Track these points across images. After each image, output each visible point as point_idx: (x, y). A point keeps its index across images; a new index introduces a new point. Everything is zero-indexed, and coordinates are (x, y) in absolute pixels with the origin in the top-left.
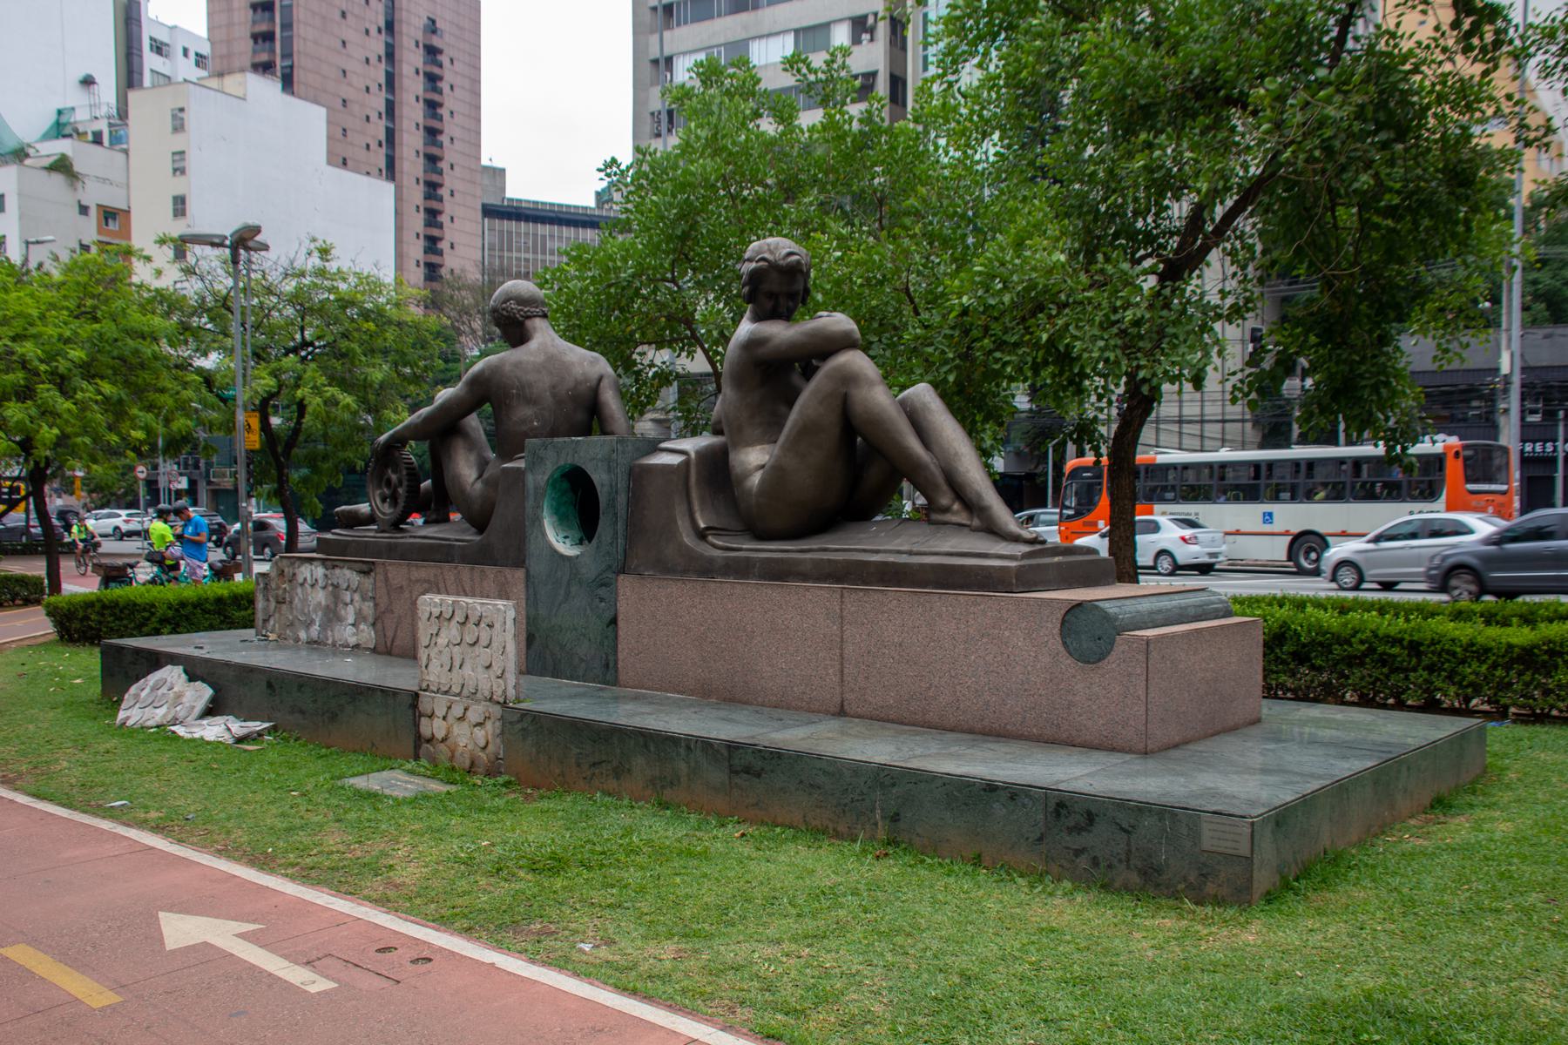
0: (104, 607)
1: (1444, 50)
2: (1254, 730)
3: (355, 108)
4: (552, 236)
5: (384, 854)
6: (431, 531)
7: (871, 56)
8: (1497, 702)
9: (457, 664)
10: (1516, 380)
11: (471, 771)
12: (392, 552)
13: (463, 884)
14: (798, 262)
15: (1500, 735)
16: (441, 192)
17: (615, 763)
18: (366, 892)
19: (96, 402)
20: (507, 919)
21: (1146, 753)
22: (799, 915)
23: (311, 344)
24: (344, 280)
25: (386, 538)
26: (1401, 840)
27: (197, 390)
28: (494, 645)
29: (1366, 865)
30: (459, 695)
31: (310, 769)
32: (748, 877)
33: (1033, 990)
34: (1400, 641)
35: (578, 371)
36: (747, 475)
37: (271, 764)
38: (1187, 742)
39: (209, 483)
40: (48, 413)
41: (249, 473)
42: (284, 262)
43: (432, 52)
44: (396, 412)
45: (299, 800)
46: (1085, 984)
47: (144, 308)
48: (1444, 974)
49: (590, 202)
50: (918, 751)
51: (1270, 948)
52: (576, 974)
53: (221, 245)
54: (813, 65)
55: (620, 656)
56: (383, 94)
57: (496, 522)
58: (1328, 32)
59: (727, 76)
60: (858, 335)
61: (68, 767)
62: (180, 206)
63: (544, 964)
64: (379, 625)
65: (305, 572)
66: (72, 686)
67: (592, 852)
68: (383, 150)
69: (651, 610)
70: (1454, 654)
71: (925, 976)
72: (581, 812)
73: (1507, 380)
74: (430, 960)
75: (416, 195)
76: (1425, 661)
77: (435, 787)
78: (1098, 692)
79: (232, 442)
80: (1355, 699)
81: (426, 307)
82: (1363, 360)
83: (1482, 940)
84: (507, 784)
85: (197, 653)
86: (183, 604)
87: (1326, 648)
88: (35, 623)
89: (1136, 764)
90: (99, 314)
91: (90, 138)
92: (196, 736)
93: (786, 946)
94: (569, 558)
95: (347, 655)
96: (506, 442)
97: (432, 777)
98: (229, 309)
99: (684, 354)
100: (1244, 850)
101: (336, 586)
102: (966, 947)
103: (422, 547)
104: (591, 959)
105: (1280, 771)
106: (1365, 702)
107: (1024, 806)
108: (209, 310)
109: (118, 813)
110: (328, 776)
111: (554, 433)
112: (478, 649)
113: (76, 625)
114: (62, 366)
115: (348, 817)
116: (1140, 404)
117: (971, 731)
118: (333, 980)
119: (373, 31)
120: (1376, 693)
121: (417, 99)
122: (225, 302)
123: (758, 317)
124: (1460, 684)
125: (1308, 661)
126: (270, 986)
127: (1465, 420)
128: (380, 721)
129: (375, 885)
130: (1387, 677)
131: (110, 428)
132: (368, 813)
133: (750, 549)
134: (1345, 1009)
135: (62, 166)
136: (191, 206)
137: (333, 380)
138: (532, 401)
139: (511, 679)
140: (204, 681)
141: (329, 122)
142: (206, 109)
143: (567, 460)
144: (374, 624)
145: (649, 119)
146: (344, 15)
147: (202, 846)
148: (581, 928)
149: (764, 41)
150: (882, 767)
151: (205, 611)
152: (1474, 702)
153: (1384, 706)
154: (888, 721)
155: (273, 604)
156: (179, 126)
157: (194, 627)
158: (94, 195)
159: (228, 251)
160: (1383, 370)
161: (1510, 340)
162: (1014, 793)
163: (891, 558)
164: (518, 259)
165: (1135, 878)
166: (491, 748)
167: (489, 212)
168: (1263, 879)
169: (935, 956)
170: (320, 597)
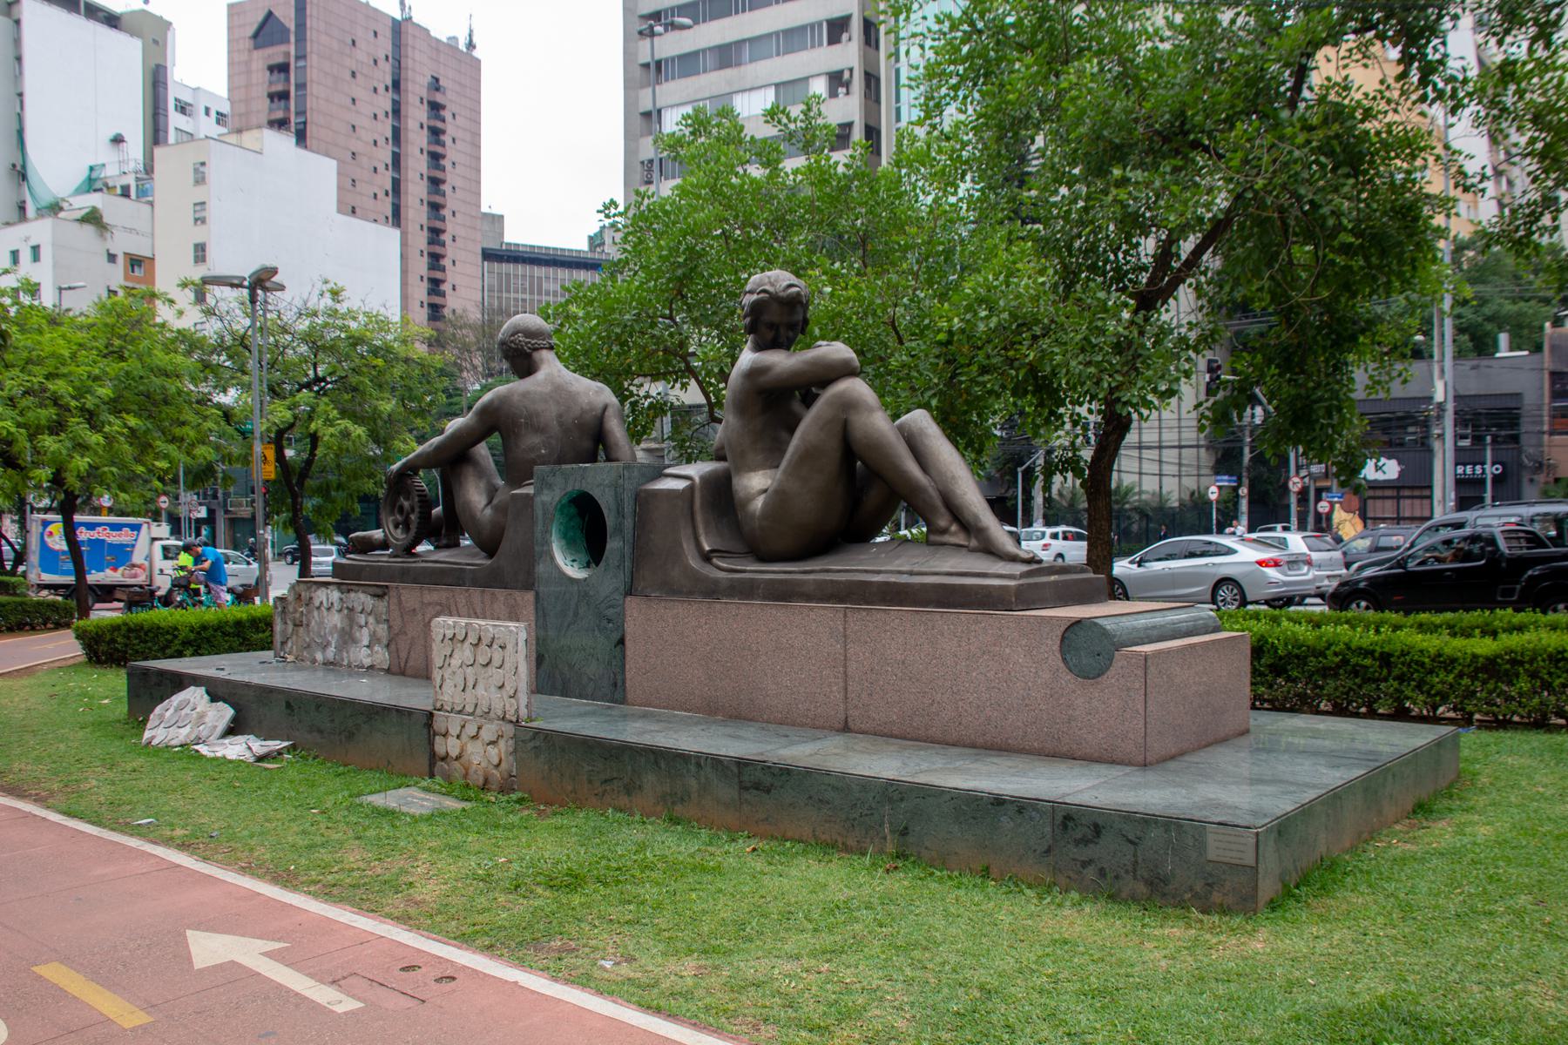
0: (130, 630)
1: (1389, 102)
2: (1243, 741)
3: (364, 160)
4: (548, 278)
5: (403, 871)
6: (443, 555)
7: (846, 109)
8: (1462, 709)
9: (470, 684)
10: (1450, 407)
11: (485, 787)
12: (406, 576)
13: (482, 901)
14: (798, 294)
15: (1471, 739)
16: (443, 237)
17: (626, 780)
18: (387, 909)
19: (122, 434)
20: (528, 936)
21: (1145, 765)
22: (815, 930)
23: (324, 379)
24: (354, 319)
25: (400, 563)
26: (1390, 845)
27: (217, 423)
28: (507, 665)
29: (1361, 871)
30: (472, 714)
31: (329, 786)
32: (762, 892)
33: (1053, 1004)
34: (1372, 653)
35: (584, 401)
36: (750, 499)
37: (291, 782)
38: (1182, 754)
39: (227, 512)
40: (81, 447)
41: (266, 503)
42: (298, 303)
43: (435, 107)
44: (404, 442)
45: (319, 818)
46: (1104, 996)
47: (169, 348)
48: (1450, 978)
49: (583, 246)
50: (924, 766)
51: (1279, 955)
52: (600, 993)
54: (793, 115)
55: (628, 676)
56: (390, 147)
57: (505, 546)
58: (1284, 83)
59: (715, 129)
60: (857, 364)
61: (97, 785)
62: (200, 253)
63: (567, 982)
64: (393, 647)
65: (321, 596)
66: (100, 706)
67: (608, 868)
68: (390, 199)
69: (659, 631)
70: (1423, 665)
71: (946, 990)
72: (595, 828)
73: (1441, 407)
74: (454, 979)
75: (420, 240)
76: (1396, 672)
77: (451, 804)
78: (1098, 706)
79: (248, 474)
80: (1329, 708)
81: (430, 345)
82: (1318, 385)
83: (1481, 943)
84: (520, 801)
85: (221, 675)
86: (204, 627)
87: (1301, 660)
88: (63, 646)
89: (1137, 776)
90: (126, 354)
91: (119, 191)
92: (219, 754)
93: (805, 962)
94: (576, 581)
95: (363, 675)
96: (515, 471)
97: (447, 794)
98: (246, 347)
99: (678, 385)
100: (1249, 859)
101: (351, 610)
102: (983, 960)
103: (433, 571)
104: (613, 977)
105: (1275, 781)
106: (1340, 711)
107: (1031, 818)
108: (228, 348)
109: (145, 830)
110: (346, 793)
111: (561, 460)
112: (491, 670)
113: (103, 647)
114: (90, 402)
115: (368, 834)
116: (1114, 429)
117: (973, 746)
118: (359, 999)
119: (381, 90)
120: (1349, 703)
122: (242, 341)
123: (759, 347)
124: (1428, 693)
125: (1289, 677)
126: (297, 1006)
127: (1402, 445)
128: (394, 740)
129: (396, 902)
130: (1360, 687)
131: (138, 460)
132: (386, 829)
133: (754, 570)
134: (1363, 1017)
136: (211, 253)
137: (344, 413)
138: (540, 430)
139: (523, 698)
140: (225, 701)
141: (339, 174)
142: (226, 163)
143: (574, 486)
144: (388, 646)
145: (639, 167)
146: (353, 74)
147: (227, 864)
148: (601, 945)
149: (746, 95)
150: (890, 783)
151: (224, 634)
152: (1441, 709)
153: (1357, 715)
154: (892, 736)
155: (290, 627)
156: (200, 179)
157: (216, 650)
158: (122, 244)
159: (245, 292)
160: (1335, 395)
161: (1442, 371)
162: (1022, 806)
163: (893, 579)
164: (516, 300)
165: (1142, 888)
166: (504, 766)
167: (489, 255)
168: (1268, 888)
169: (954, 971)
170: (335, 619)
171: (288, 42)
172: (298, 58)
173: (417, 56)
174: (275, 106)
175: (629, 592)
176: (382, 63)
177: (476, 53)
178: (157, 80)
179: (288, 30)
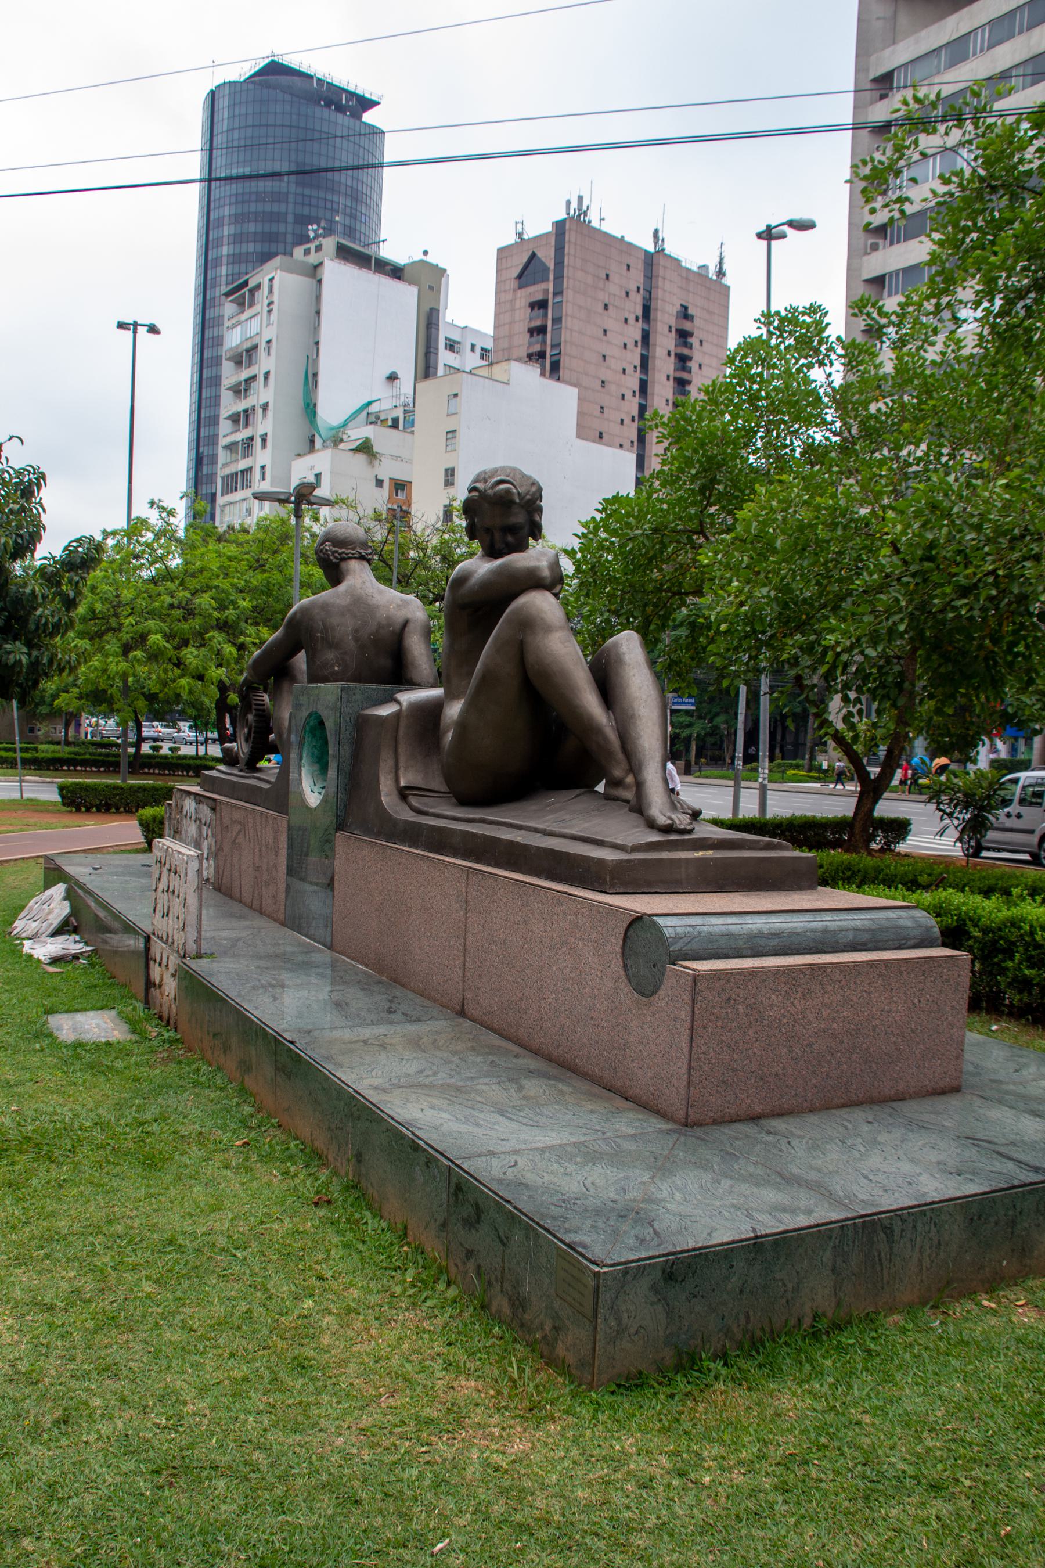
3: (612, 388)
53: (286, 501)
56: (638, 375)
91: (390, 423)
121: (668, 377)
135: (365, 448)
158: (388, 470)
171: (548, 280)
172: (555, 294)
173: (668, 286)
174: (533, 339)
175: (340, 827)
176: (633, 294)
177: (726, 281)
178: (429, 322)
179: (547, 269)
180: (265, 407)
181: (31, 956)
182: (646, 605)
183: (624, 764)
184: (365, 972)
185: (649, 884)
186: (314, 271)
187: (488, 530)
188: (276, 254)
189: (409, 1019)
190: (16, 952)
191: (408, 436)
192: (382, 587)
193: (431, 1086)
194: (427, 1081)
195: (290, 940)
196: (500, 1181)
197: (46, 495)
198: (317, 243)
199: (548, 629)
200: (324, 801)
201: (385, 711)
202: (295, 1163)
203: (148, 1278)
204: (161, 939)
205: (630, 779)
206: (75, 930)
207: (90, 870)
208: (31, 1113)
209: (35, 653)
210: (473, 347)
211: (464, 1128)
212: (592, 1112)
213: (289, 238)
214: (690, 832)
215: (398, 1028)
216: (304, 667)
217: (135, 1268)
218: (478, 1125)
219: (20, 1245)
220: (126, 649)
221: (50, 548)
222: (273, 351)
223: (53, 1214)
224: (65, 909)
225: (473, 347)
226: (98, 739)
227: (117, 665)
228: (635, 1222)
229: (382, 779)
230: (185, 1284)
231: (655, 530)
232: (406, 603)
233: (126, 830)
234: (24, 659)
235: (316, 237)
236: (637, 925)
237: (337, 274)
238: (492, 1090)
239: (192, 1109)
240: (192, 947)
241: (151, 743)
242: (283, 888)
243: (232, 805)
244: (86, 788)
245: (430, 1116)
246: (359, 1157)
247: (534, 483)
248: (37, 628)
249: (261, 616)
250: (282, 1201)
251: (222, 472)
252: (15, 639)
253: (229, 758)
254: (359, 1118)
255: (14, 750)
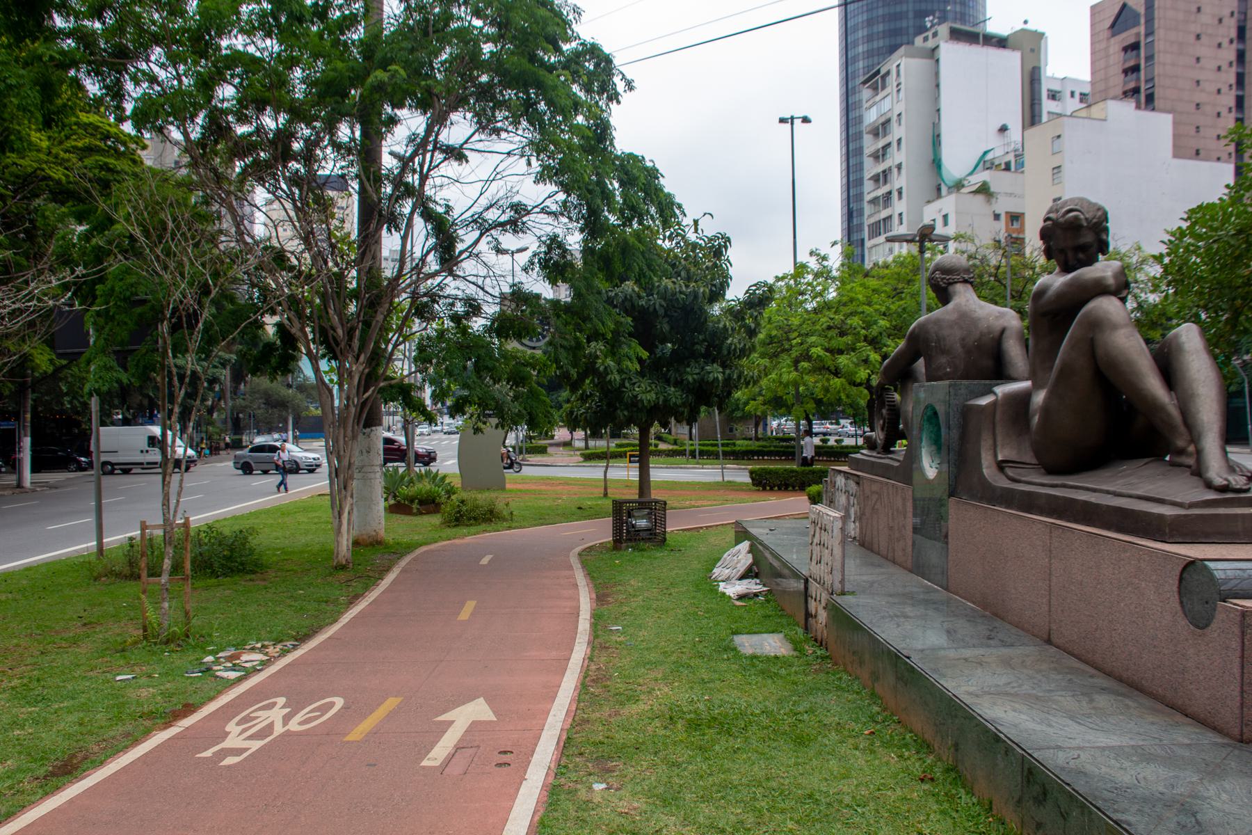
3: (1207, 109)
138: (944, 352)
146: (1198, 37)
172: (1147, 35)
175: (952, 494)
178: (1032, 78)
180: (899, 167)
181: (724, 594)
182: (1234, 299)
183: (1186, 436)
184: (972, 609)
185: (1207, 535)
186: (933, 53)
187: (1062, 251)
188: (901, 45)
189: (1004, 644)
190: (714, 590)
191: (1020, 176)
192: (983, 303)
193: (1016, 695)
194: (1012, 691)
195: (916, 583)
196: (1063, 769)
197: (731, 253)
198: (933, 30)
199: (1115, 327)
200: (939, 473)
201: (984, 401)
202: (909, 750)
203: (791, 819)
204: (815, 580)
205: (1191, 448)
206: (757, 576)
207: (767, 531)
208: (717, 702)
209: (728, 372)
210: (1072, 94)
211: (1038, 727)
212: (1153, 723)
213: (911, 31)
214: (1247, 491)
215: (994, 651)
216: (923, 370)
217: (783, 811)
218: (1050, 726)
219: (705, 788)
220: (796, 362)
221: (736, 292)
222: (903, 121)
223: (729, 770)
224: (749, 560)
225: (1072, 94)
226: (781, 435)
227: (790, 376)
228: (1179, 811)
229: (983, 455)
230: (818, 826)
231: (1240, 232)
232: (1002, 315)
233: (797, 503)
234: (720, 377)
235: (932, 26)
236: (1190, 568)
237: (953, 54)
238: (1068, 701)
239: (834, 706)
240: (837, 586)
241: (821, 437)
242: (910, 543)
243: (871, 480)
244: (770, 472)
245: (1013, 718)
246: (956, 746)
247: (1100, 208)
248: (729, 353)
249: (897, 331)
250: (895, 776)
251: (867, 221)
252: (713, 362)
253: (871, 444)
254: (956, 716)
255: (717, 445)
